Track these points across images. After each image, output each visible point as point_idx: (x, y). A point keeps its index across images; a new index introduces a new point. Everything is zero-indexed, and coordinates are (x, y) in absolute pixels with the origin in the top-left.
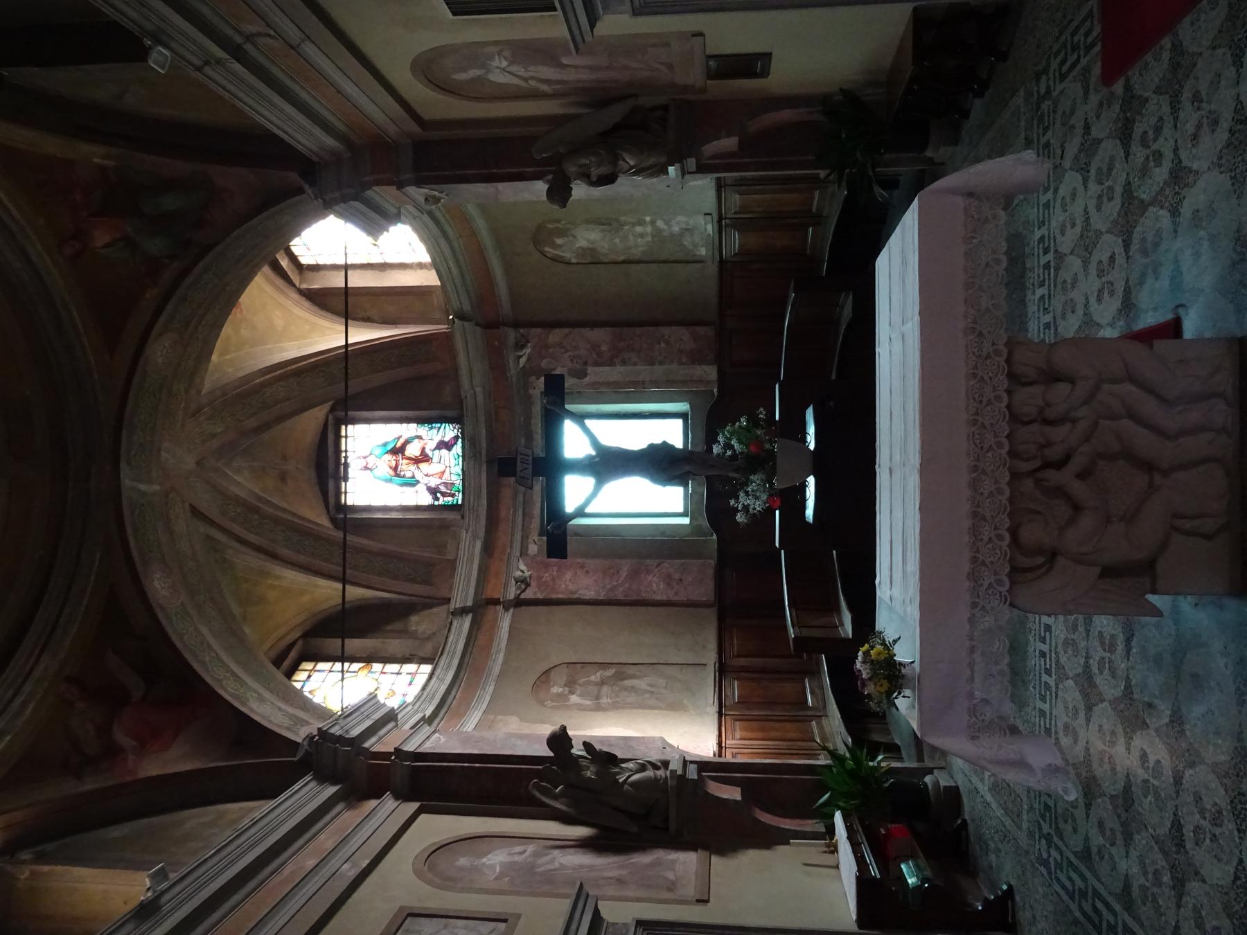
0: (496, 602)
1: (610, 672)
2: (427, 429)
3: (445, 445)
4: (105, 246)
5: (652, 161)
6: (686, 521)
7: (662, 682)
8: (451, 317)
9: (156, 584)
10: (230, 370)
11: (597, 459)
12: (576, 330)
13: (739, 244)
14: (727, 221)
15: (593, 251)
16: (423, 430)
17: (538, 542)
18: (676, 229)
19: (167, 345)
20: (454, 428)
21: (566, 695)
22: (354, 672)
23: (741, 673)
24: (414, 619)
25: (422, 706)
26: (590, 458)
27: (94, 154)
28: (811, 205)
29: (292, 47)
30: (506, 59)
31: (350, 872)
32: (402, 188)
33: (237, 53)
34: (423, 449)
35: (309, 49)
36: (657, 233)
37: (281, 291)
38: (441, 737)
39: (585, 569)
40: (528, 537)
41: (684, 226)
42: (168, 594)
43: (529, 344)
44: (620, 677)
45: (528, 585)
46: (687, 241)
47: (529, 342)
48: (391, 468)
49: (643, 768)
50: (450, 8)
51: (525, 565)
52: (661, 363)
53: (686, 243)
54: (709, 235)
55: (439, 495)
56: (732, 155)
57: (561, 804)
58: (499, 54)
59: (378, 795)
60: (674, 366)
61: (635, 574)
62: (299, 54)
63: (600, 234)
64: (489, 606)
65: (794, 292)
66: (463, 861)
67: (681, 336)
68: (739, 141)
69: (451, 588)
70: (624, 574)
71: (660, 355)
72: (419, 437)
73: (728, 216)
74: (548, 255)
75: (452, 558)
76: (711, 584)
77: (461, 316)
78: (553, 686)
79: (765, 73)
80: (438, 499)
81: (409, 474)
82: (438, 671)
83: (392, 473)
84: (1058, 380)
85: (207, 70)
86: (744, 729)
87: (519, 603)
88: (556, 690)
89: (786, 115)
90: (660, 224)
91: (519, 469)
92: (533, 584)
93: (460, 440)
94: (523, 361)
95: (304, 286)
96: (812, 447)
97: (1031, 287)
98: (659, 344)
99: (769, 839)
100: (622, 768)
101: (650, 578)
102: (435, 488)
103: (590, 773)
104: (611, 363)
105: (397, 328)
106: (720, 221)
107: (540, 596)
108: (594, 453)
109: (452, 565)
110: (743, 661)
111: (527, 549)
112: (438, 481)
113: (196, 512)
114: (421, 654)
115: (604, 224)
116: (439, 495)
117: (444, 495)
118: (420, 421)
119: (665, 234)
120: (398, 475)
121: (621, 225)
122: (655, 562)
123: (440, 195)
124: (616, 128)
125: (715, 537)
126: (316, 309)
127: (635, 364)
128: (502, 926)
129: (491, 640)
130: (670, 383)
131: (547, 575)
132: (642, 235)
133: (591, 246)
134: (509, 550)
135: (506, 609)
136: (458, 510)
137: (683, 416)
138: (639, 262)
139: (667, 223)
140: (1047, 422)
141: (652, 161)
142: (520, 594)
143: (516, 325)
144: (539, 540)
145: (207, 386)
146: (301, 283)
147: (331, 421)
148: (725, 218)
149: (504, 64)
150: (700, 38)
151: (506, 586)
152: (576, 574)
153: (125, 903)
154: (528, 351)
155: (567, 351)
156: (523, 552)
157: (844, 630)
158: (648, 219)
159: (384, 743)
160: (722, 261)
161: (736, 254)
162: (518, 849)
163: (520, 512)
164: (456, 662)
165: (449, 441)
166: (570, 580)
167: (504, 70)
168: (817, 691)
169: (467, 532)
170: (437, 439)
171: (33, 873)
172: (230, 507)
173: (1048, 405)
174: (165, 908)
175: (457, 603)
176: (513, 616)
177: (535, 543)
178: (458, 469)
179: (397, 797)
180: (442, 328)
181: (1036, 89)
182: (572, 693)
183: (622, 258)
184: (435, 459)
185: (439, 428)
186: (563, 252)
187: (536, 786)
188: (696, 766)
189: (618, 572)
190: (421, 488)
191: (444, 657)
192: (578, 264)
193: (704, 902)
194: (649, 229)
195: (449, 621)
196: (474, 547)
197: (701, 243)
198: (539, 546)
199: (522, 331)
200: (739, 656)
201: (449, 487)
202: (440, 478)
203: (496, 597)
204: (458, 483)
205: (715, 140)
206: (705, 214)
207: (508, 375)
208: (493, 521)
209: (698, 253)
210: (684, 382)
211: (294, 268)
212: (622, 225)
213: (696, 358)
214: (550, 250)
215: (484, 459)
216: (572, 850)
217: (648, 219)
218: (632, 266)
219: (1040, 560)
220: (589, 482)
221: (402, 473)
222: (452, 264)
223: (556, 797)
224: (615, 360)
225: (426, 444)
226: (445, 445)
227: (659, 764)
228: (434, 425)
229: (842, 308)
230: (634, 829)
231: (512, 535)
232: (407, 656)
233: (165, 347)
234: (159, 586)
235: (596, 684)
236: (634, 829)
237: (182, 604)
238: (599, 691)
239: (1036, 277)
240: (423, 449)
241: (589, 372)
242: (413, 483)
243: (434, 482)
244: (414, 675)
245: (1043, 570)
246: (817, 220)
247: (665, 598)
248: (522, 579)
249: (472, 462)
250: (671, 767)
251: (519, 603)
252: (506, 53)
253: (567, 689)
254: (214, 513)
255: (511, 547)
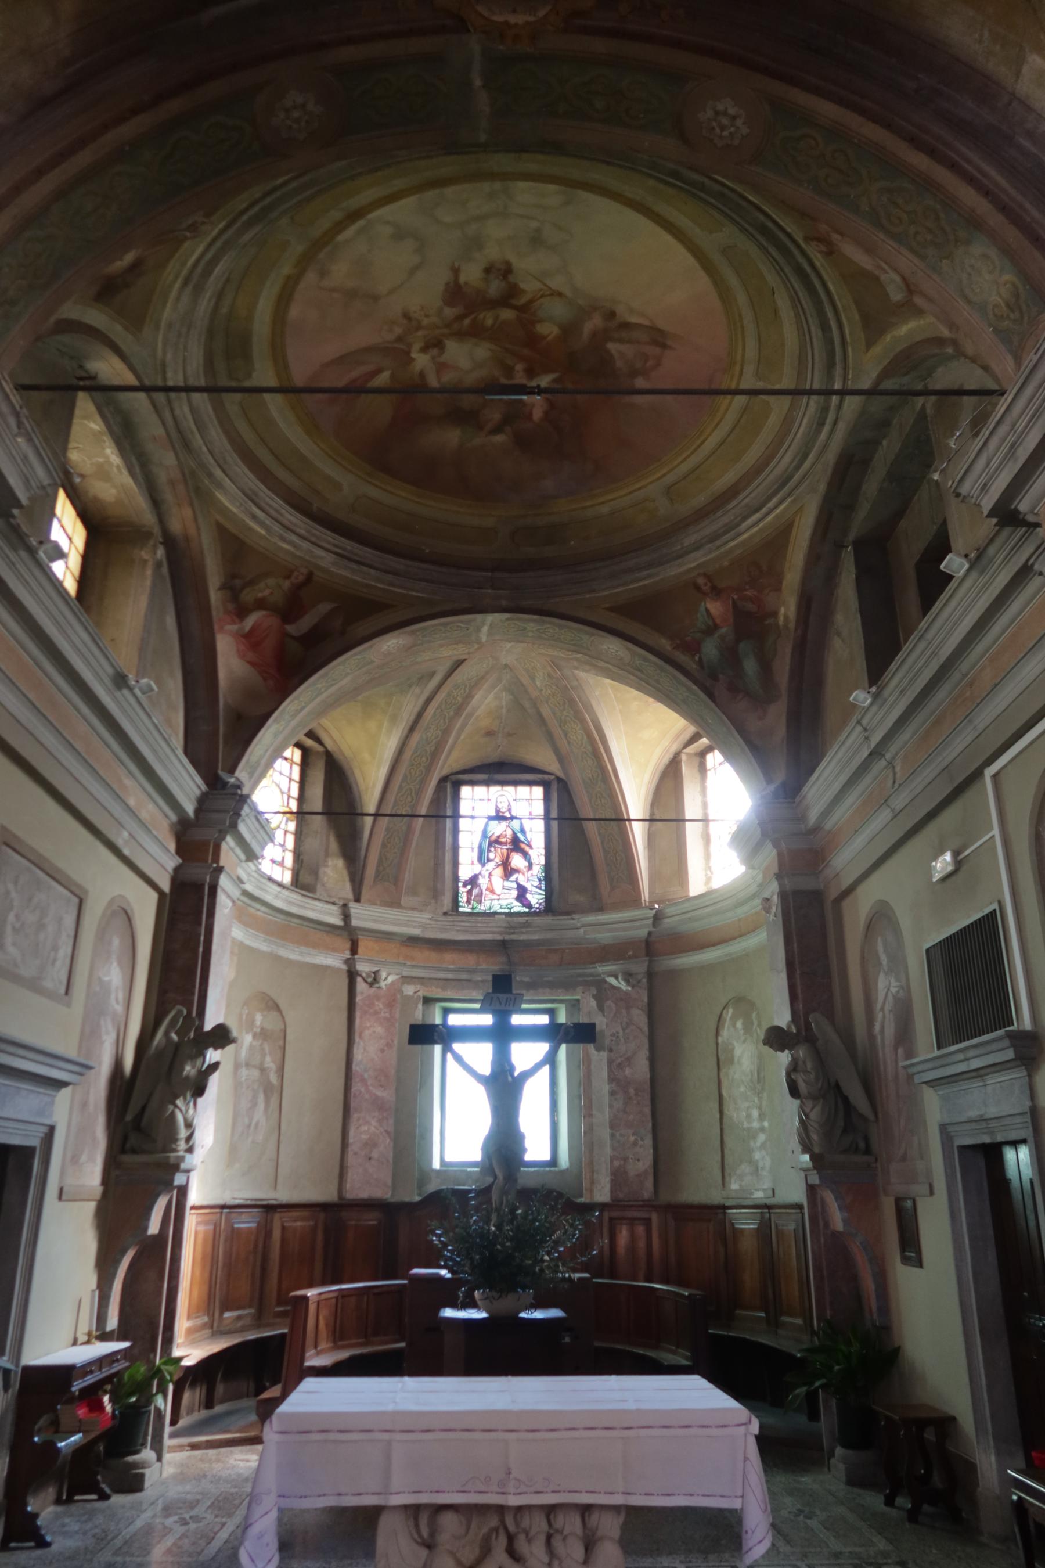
0: (354, 951)
1: (274, 1078)
2: (540, 875)
3: (522, 893)
4: (707, 611)
5: (815, 1137)
6: (436, 1165)
7: (260, 1138)
8: (657, 906)
9: (394, 641)
10: (597, 693)
11: (510, 1079)
12: (646, 1041)
13: (745, 1229)
14: (768, 1215)
15: (731, 1061)
16: (538, 870)
17: (416, 994)
18: (757, 1156)
19: (619, 653)
20: (540, 904)
21: (252, 1030)
22: (288, 803)
23: (265, 1230)
24: (340, 863)
25: (253, 880)
26: (512, 1068)
27: (787, 609)
28: (790, 1316)
29: (886, 801)
30: (898, 992)
31: (121, 840)
32: (776, 878)
33: (876, 753)
34: (517, 871)
35: (885, 815)
36: (752, 1134)
37: (678, 736)
38: (228, 909)
39: (386, 1048)
40: (422, 984)
41: (761, 1164)
42: (383, 650)
43: (630, 989)
44: (268, 1089)
45: (371, 985)
46: (745, 1168)
47: (633, 987)
48: (499, 837)
49: (189, 1125)
50: (931, 947)
51: (393, 983)
52: (612, 1136)
53: (743, 1167)
54: (752, 1193)
55: (469, 887)
56: (827, 1225)
57: (160, 1039)
58: (902, 987)
59: (179, 851)
60: (608, 1151)
61: (379, 1105)
62: (881, 806)
63: (748, 1069)
64: (350, 943)
65: (690, 1295)
66: (116, 942)
67: (642, 1161)
68: (839, 1232)
69: (372, 903)
70: (380, 1093)
71: (622, 1135)
72: (530, 867)
73: (772, 1215)
74: (724, 1012)
75: (402, 903)
76: (364, 1194)
77: (658, 918)
78: (262, 1015)
79: (905, 1260)
80: (465, 886)
81: (492, 856)
82: (286, 893)
83: (493, 838)
84: (587, 1549)
85: (859, 729)
86: (206, 1232)
87: (352, 975)
88: (259, 1018)
89: (869, 1285)
90: (762, 1137)
91: (501, 996)
92: (373, 990)
93: (527, 910)
94: (612, 981)
95: (684, 757)
96: (522, 1315)
97: (688, 1560)
98: (633, 1134)
99: (105, 1265)
100: (189, 1102)
101: (374, 1123)
102: (476, 883)
103: (189, 1070)
104: (611, 1079)
105: (645, 848)
106: (769, 1207)
107: (359, 998)
108: (516, 1074)
109: (395, 903)
110: (277, 1234)
111: (409, 983)
112: (483, 887)
113: (459, 663)
114: (302, 873)
115: (758, 1074)
116: (469, 887)
117: (469, 892)
118: (547, 868)
119: (752, 1143)
120: (490, 845)
121: (758, 1094)
122: (391, 1129)
123: (773, 914)
124: (846, 1100)
125: (417, 1199)
126: (662, 767)
127: (611, 1106)
128: (63, 991)
129: (315, 945)
130: (591, 1147)
131: (381, 1006)
132: (749, 1116)
133: (736, 1060)
134: (409, 963)
135: (347, 962)
136: (452, 908)
137: (554, 1161)
138: (721, 1112)
139: (763, 1146)
140: (549, 1538)
141: (815, 1137)
142: (361, 976)
143: (651, 975)
144: (419, 996)
145: (581, 674)
146: (687, 754)
147: (546, 777)
148: (770, 1213)
149: (893, 990)
150: (928, 1192)
151: (370, 961)
152: (381, 1038)
153: (113, 640)
154: (623, 986)
155: (624, 1030)
156: (407, 979)
157: (312, 1357)
158: (766, 1124)
159: (229, 850)
160: (724, 1207)
161: (733, 1224)
162: (121, 996)
163: (450, 976)
164: (294, 910)
165: (527, 899)
166: (374, 1032)
167: (889, 989)
168: (240, 1324)
169: (430, 919)
170: (528, 886)
171: (145, 562)
172: (462, 691)
173: (564, 1539)
174: (118, 694)
175: (355, 909)
176: (339, 969)
177: (415, 993)
178: (496, 908)
179: (177, 870)
180: (645, 895)
181: (889, 1561)
182: (255, 1036)
183: (725, 1094)
184: (507, 884)
185: (540, 888)
186: (729, 1028)
187: (180, 1012)
188: (184, 1183)
189: (381, 1086)
190: (477, 868)
191: (299, 897)
192: (717, 1044)
193: (60, 1198)
194: (755, 1125)
195: (337, 902)
196: (414, 927)
197: (743, 1184)
198: (412, 997)
199: (645, 980)
200: (284, 1228)
201: (477, 898)
202: (487, 889)
203: (360, 950)
204: (482, 908)
205: (839, 1206)
206: (773, 1190)
207: (597, 965)
208: (440, 945)
209: (733, 1180)
210: (591, 1163)
211: (702, 748)
212: (759, 1094)
213: (618, 1177)
214: (730, 1015)
215: (507, 937)
216: (114, 1051)
217: (766, 1124)
218: (717, 1105)
219: (425, 1532)
220: (485, 1068)
221: (493, 849)
222: (710, 909)
223: (167, 1034)
224: (614, 1083)
225: (524, 874)
226: (522, 893)
227: (191, 1143)
228: (543, 882)
229: (674, 1353)
230: (129, 1118)
231: (424, 967)
232: (301, 857)
233: (617, 651)
234: (391, 643)
235: (262, 1063)
236: (129, 1118)
237: (373, 662)
238: (254, 1066)
239: (698, 1564)
240: (517, 871)
241: (602, 1053)
242: (483, 859)
243: (483, 882)
244: (281, 864)
245: (416, 1536)
246: (774, 1323)
247: (351, 1140)
248: (378, 979)
249: (504, 925)
250: (188, 1156)
251: (352, 975)
252: (901, 994)
253: (258, 1030)
254: (458, 677)
255: (413, 966)
